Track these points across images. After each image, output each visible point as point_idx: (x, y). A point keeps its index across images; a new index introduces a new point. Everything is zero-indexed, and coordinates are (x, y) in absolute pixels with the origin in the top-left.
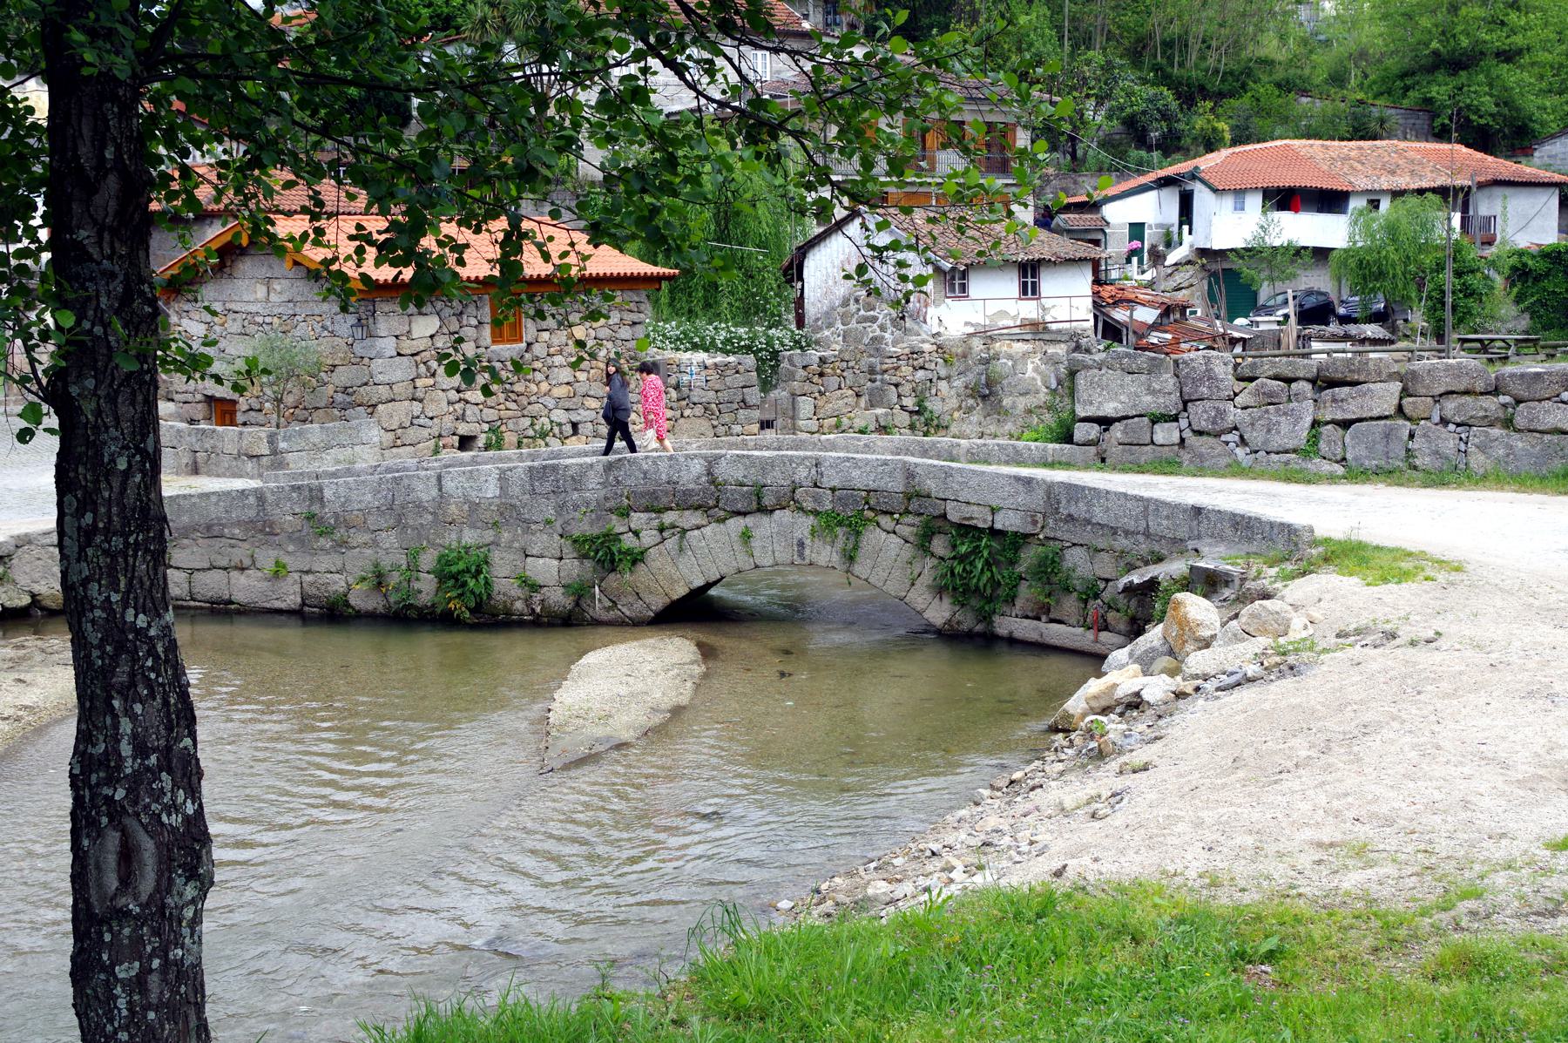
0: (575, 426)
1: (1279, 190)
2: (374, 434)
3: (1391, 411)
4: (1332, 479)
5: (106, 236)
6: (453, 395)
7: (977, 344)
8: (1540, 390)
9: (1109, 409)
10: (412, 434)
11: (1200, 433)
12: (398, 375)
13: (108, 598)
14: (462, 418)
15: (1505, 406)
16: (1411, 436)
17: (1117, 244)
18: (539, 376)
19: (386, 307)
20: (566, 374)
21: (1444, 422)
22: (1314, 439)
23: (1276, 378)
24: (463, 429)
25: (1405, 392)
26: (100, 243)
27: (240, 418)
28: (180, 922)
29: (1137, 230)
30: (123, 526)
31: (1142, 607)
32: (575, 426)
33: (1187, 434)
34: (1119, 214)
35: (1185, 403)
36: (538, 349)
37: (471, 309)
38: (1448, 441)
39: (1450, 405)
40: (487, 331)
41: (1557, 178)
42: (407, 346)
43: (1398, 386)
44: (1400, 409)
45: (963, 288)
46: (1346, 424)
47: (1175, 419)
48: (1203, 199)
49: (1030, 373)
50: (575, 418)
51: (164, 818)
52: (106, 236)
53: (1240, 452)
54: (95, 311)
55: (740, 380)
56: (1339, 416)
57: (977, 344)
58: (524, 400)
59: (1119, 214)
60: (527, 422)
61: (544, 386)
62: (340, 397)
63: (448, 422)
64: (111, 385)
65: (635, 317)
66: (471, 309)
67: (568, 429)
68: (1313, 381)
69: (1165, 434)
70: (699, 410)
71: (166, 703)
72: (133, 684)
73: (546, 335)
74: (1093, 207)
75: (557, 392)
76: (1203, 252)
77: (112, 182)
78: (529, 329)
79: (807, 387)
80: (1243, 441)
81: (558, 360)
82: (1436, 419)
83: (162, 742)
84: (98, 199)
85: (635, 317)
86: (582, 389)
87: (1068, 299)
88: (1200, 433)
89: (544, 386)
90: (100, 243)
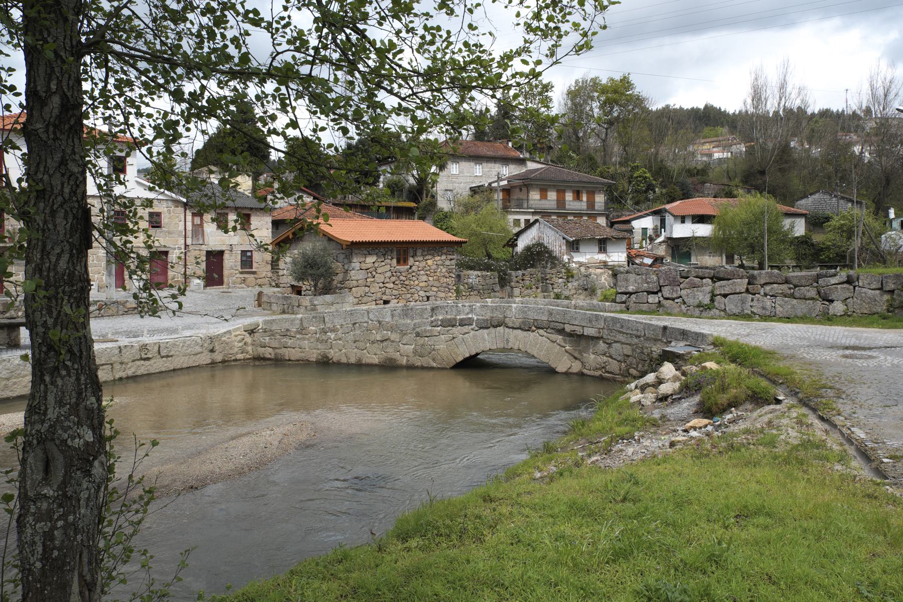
0: (428, 298)
1: (698, 216)
2: (351, 299)
3: (743, 290)
4: (721, 318)
5: (51, 129)
6: (381, 285)
7: (583, 269)
8: (803, 282)
9: (631, 288)
10: (365, 299)
11: (667, 299)
12: (361, 277)
13: (45, 322)
14: (384, 294)
15: (790, 289)
16: (752, 300)
17: (637, 236)
18: (414, 278)
19: (357, 251)
20: (425, 278)
21: (766, 295)
22: (712, 300)
23: (696, 277)
24: (385, 298)
25: (749, 283)
26: (47, 132)
27: (303, 293)
28: (79, 500)
29: (645, 230)
30: (56, 282)
31: (696, 412)
32: (428, 298)
33: (661, 299)
34: (639, 225)
35: (661, 287)
36: (414, 268)
37: (389, 253)
38: (768, 302)
39: (768, 288)
40: (395, 261)
41: (804, 212)
42: (364, 266)
43: (747, 280)
44: (747, 291)
45: (577, 249)
46: (725, 296)
47: (656, 293)
48: (669, 219)
49: (603, 280)
50: (428, 294)
51: (69, 442)
52: (51, 129)
53: (683, 307)
54: (45, 167)
55: (492, 281)
56: (723, 292)
57: (583, 269)
58: (408, 287)
59: (639, 225)
60: (409, 296)
61: (416, 282)
62: (339, 285)
63: (379, 295)
64: (52, 207)
65: (452, 257)
66: (389, 253)
67: (425, 299)
68: (712, 279)
69: (653, 299)
70: (476, 293)
71: (78, 379)
72: (56, 369)
73: (417, 263)
74: (628, 222)
75: (421, 284)
76: (670, 239)
77: (56, 100)
78: (411, 261)
79: (517, 284)
80: (684, 303)
81: (422, 272)
82: (762, 293)
83: (74, 400)
84: (47, 109)
85: (452, 257)
86: (431, 283)
87: (617, 256)
88: (667, 299)
89: (416, 282)
90: (47, 132)
